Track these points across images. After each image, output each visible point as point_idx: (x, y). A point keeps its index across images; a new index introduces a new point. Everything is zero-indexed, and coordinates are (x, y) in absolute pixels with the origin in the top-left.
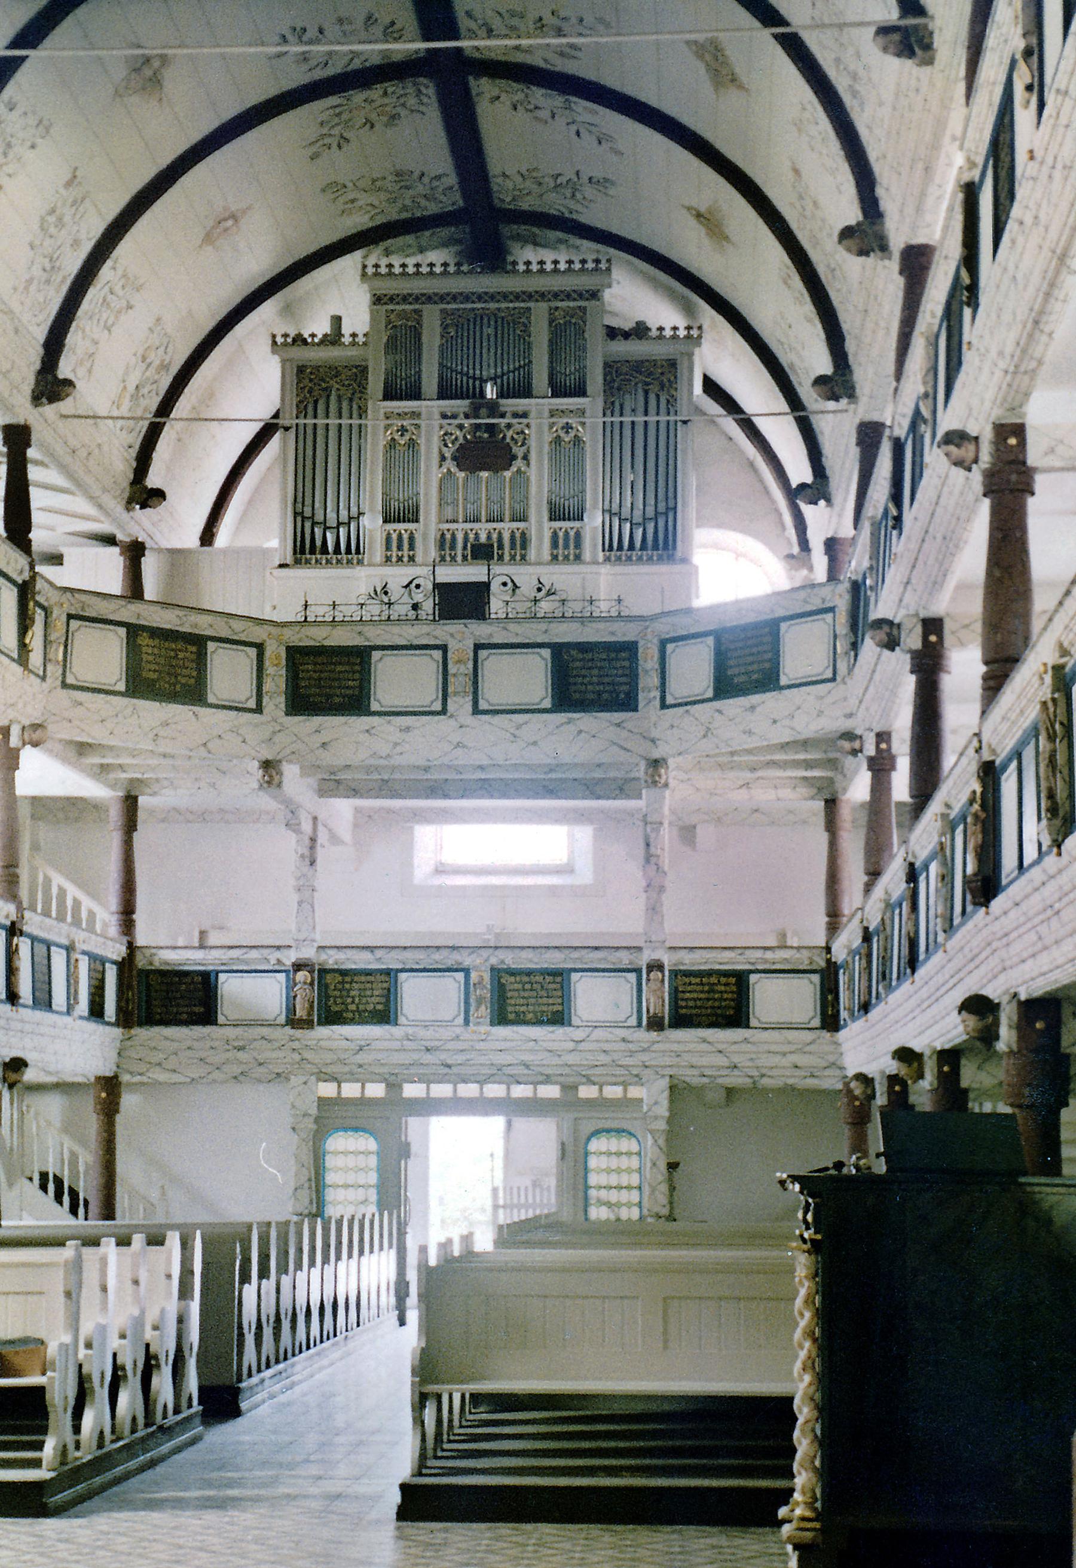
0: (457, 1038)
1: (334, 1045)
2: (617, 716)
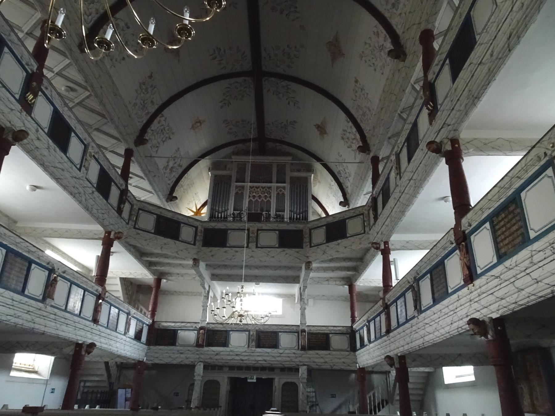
0: (245, 352)
1: (209, 353)
2: (297, 250)
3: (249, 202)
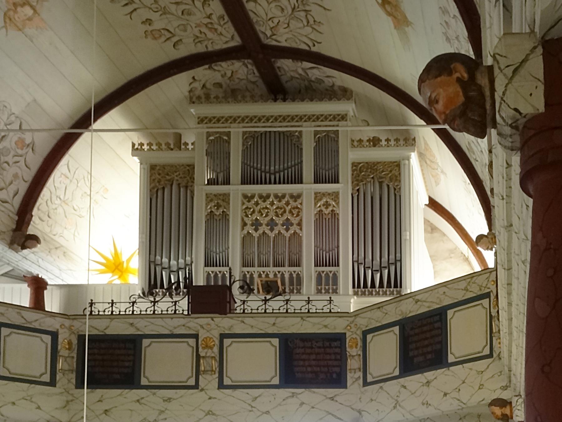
2: (331, 392)
3: (243, 239)
